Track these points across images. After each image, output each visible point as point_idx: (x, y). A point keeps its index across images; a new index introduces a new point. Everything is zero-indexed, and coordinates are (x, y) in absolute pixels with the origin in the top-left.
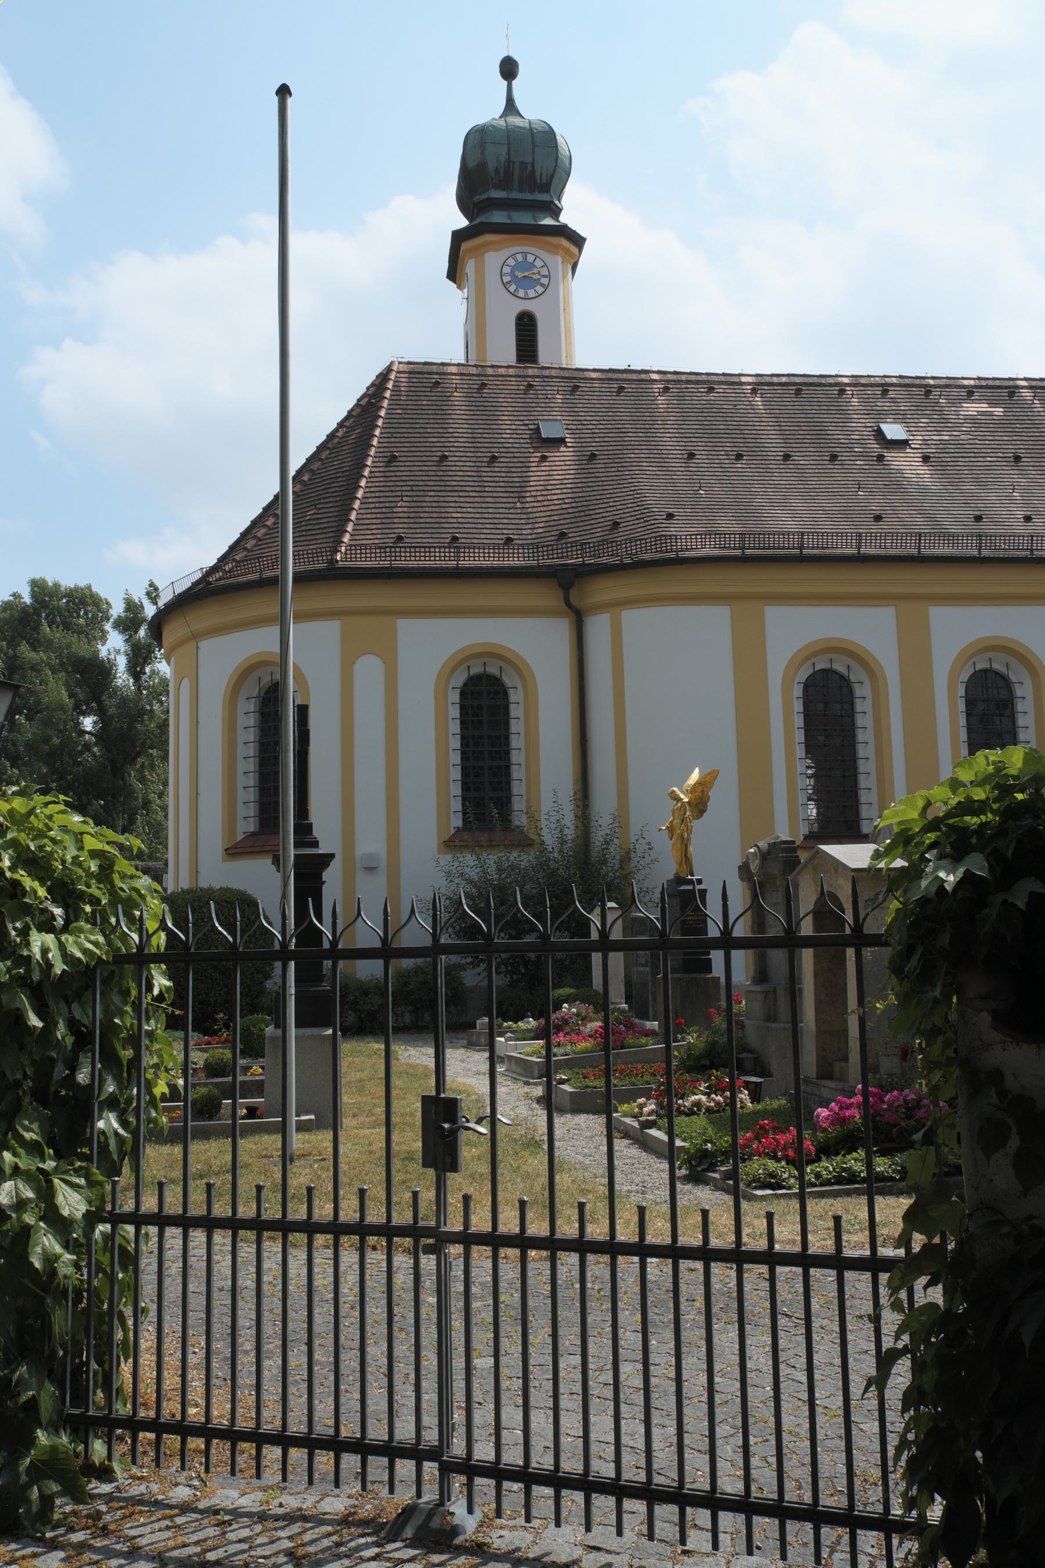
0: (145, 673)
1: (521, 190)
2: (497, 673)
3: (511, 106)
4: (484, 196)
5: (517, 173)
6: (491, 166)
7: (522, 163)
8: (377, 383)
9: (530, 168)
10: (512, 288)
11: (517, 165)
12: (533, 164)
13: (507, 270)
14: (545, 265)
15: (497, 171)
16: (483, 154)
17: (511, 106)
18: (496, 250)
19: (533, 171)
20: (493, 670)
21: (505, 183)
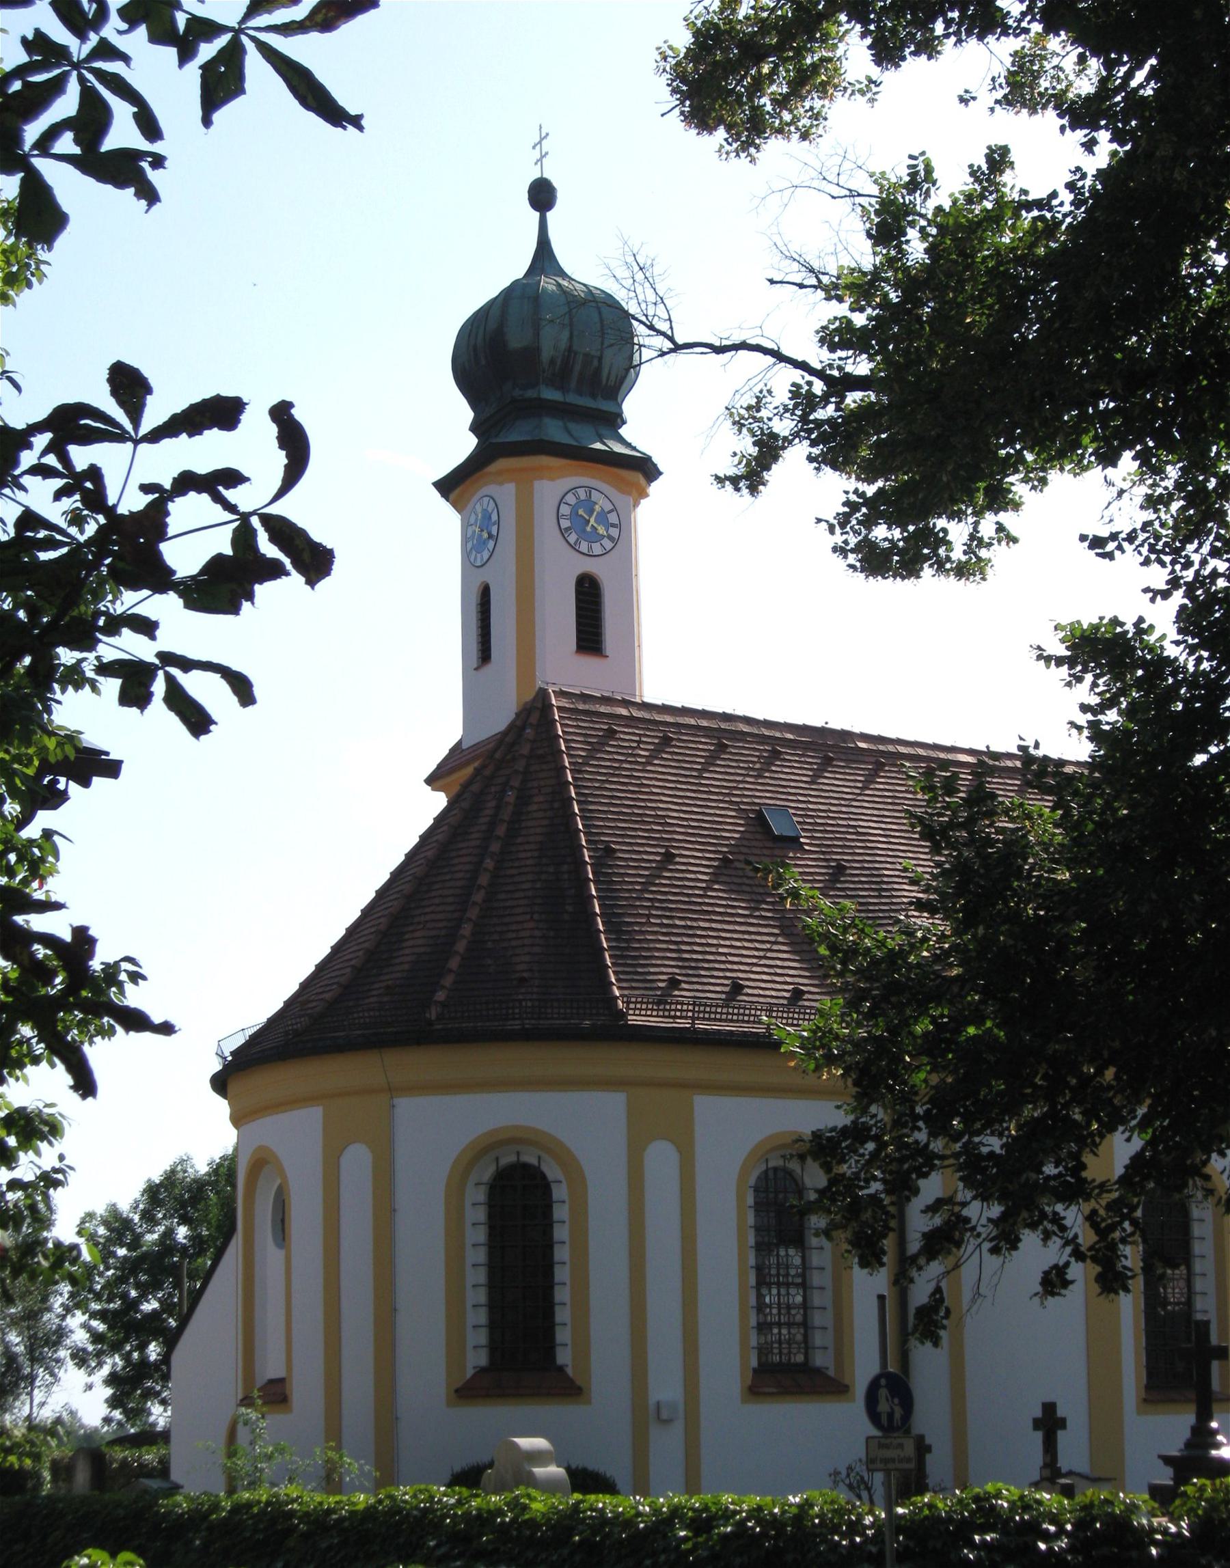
0: (49, 1309)
1: (580, 393)
2: (534, 1161)
3: (544, 255)
4: (530, 394)
5: (577, 368)
6: (547, 353)
7: (586, 355)
8: (518, 723)
9: (596, 363)
10: (572, 538)
11: (580, 358)
12: (600, 359)
13: (565, 510)
14: (615, 509)
15: (552, 362)
16: (537, 334)
17: (544, 255)
18: (552, 479)
19: (598, 370)
20: (508, 1159)
21: (560, 378)
